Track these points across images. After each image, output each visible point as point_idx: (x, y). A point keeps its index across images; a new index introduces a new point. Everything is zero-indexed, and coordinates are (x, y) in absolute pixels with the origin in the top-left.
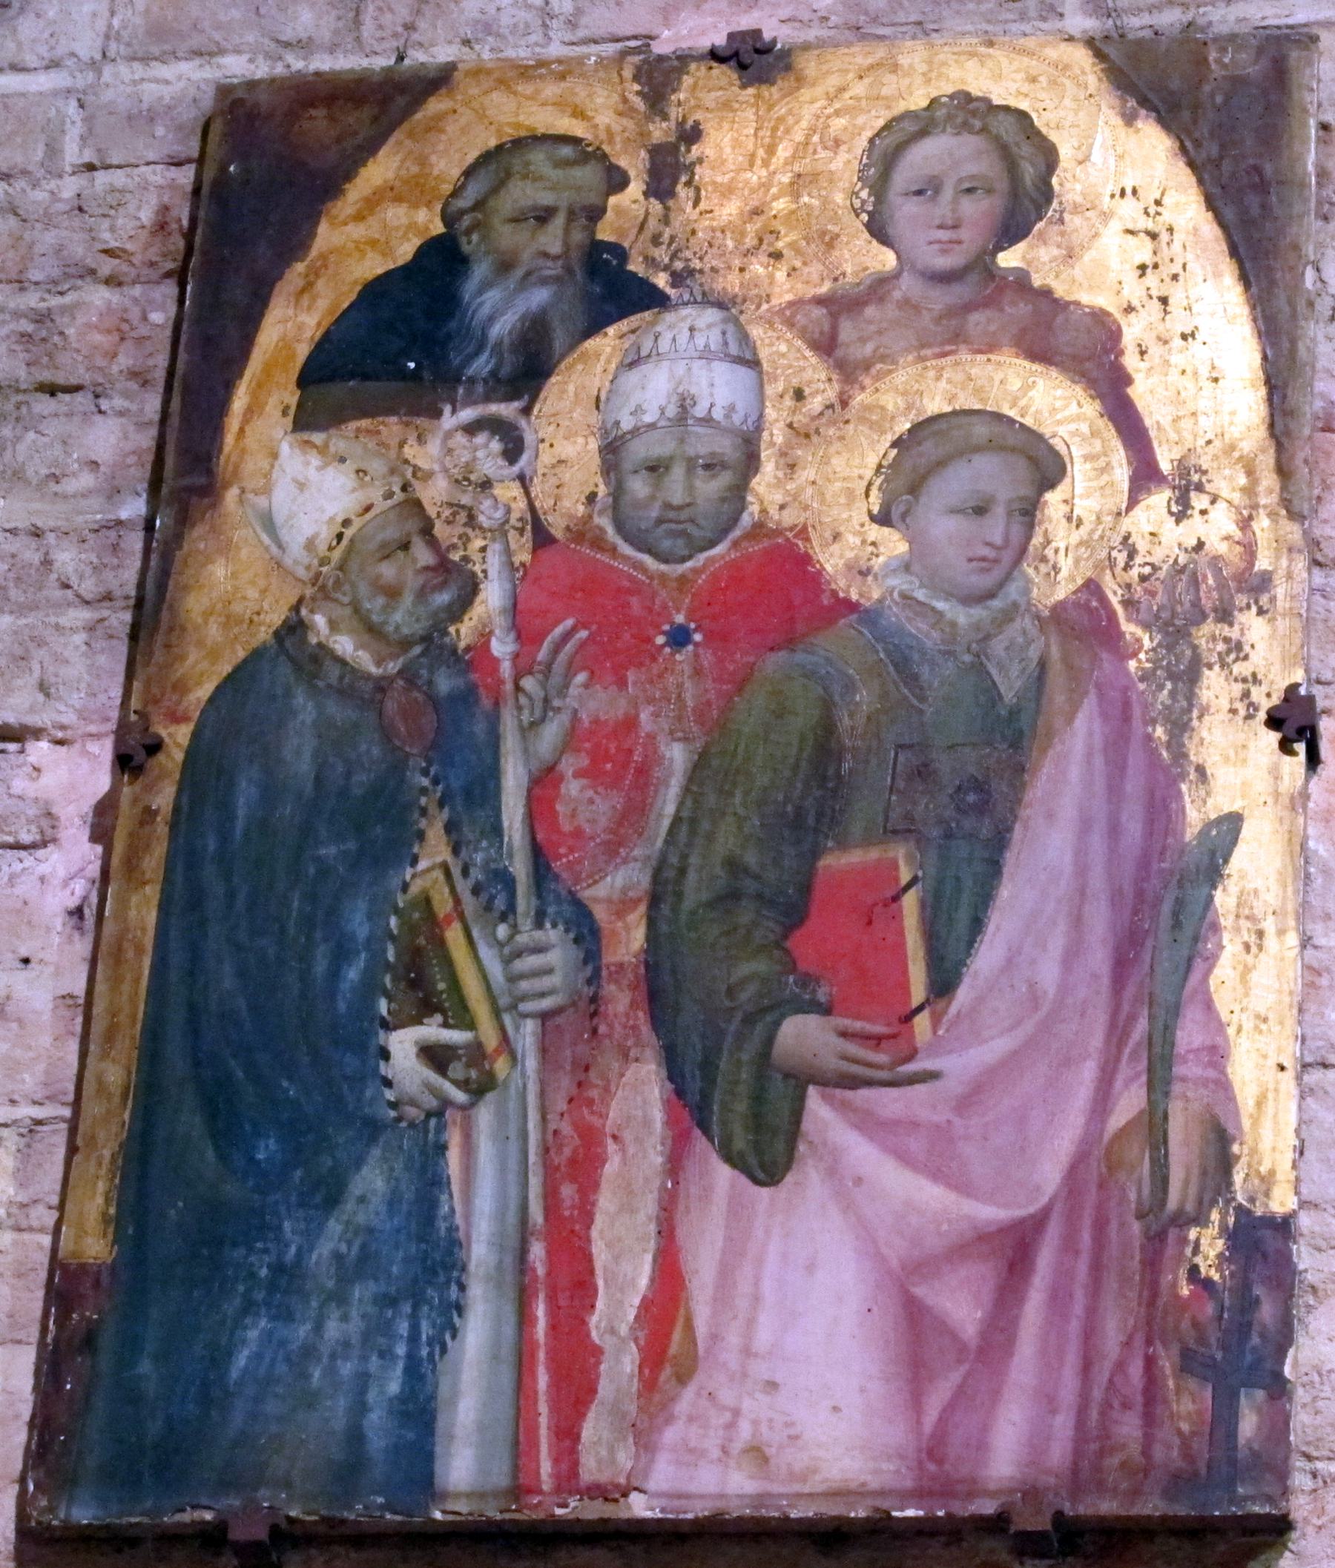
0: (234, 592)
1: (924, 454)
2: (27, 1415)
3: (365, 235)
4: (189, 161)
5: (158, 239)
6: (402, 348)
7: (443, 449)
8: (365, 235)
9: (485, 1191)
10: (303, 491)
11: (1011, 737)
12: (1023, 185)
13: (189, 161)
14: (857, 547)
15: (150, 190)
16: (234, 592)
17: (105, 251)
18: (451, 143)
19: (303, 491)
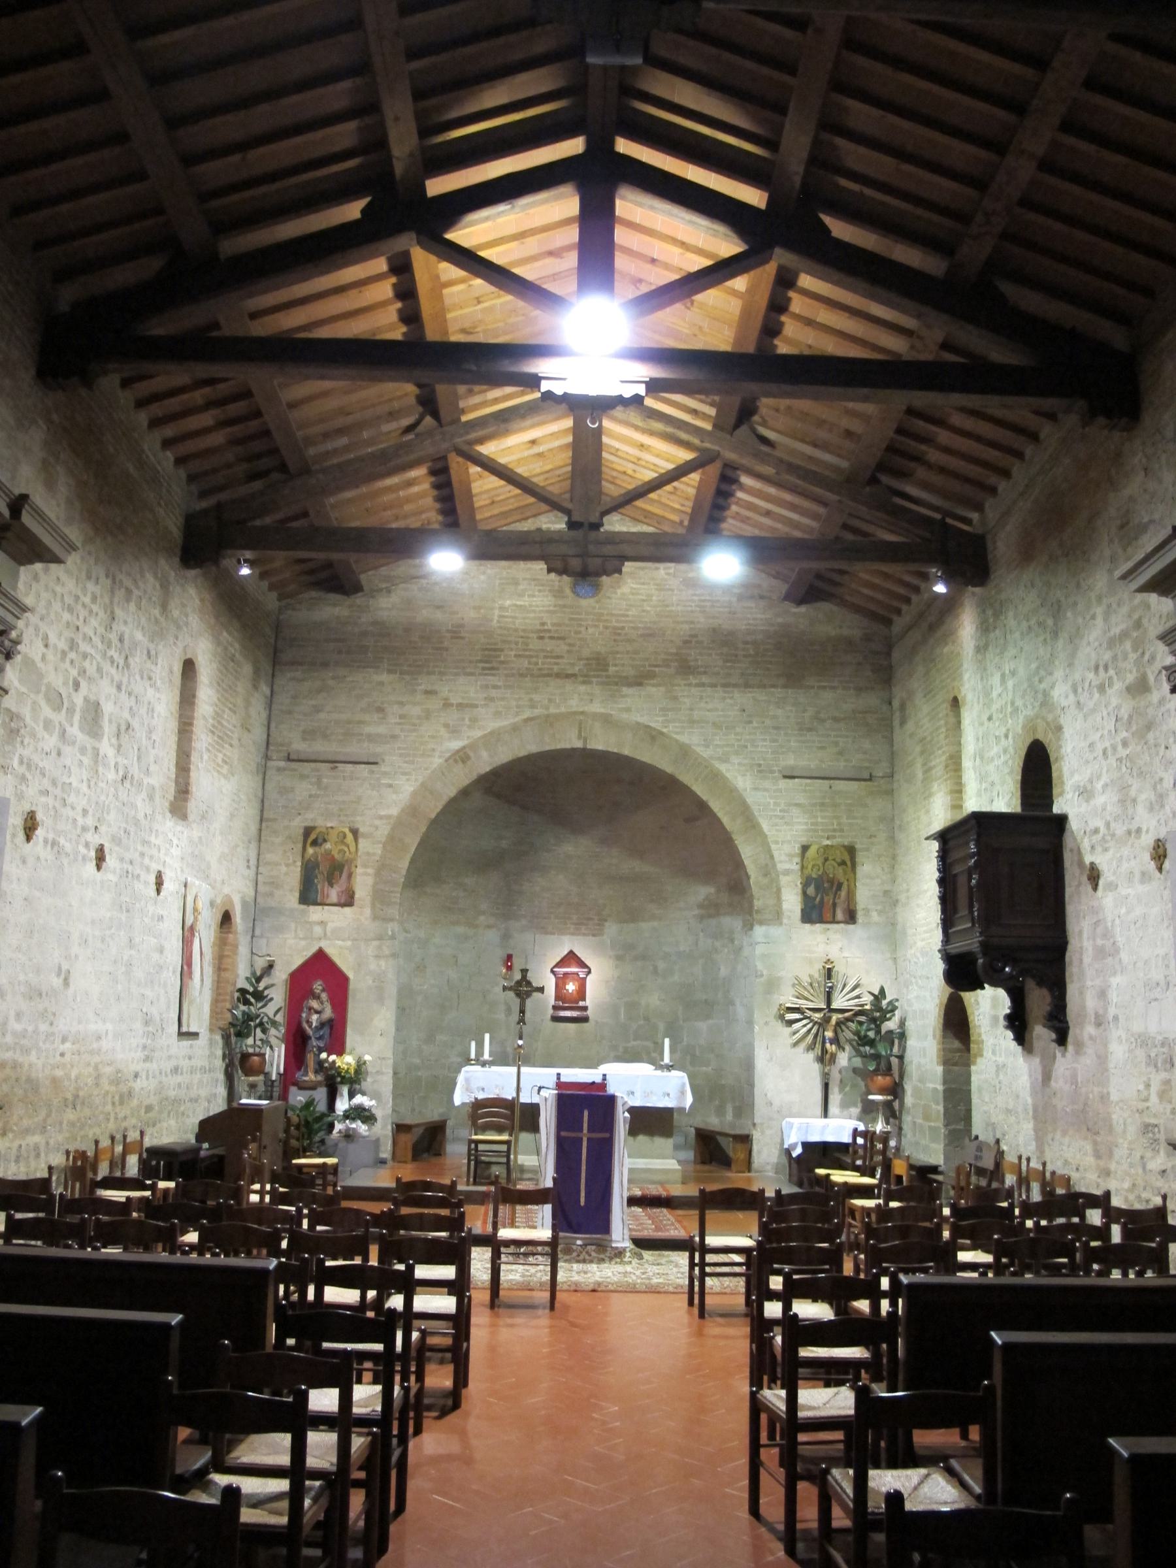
0: (307, 856)
1: (340, 851)
2: (295, 966)
3: (313, 837)
4: (411, 317)
5: (696, 411)
6: (315, 843)
7: (317, 849)
8: (313, 837)
9: (319, 887)
10: (310, 851)
11: (343, 866)
12: (345, 836)
13: (411, 317)
14: (336, 856)
15: (302, 831)
16: (307, 856)
17: (158, 891)
18: (318, 831)
19: (310, 850)
